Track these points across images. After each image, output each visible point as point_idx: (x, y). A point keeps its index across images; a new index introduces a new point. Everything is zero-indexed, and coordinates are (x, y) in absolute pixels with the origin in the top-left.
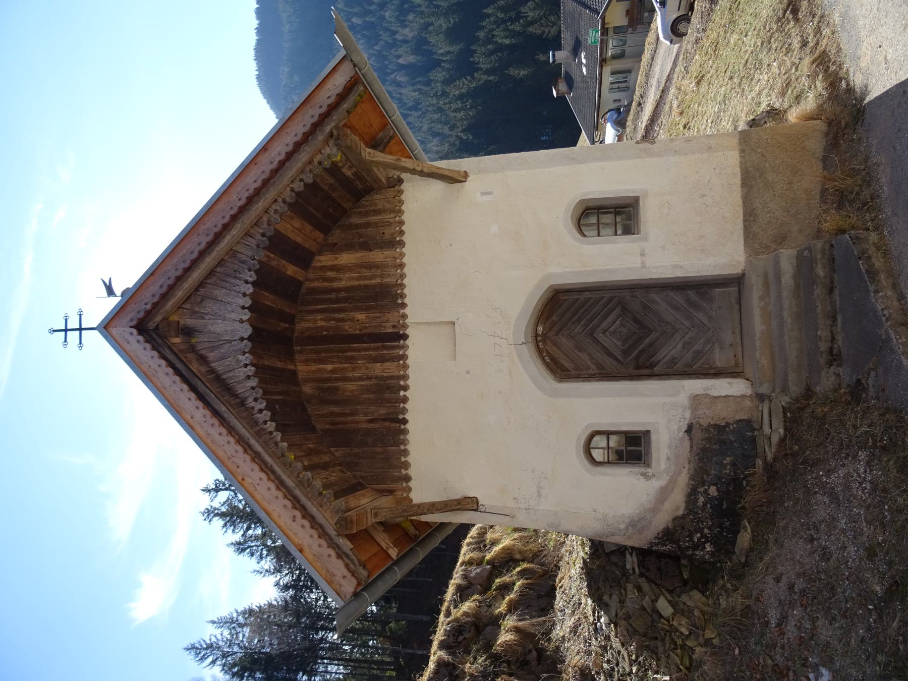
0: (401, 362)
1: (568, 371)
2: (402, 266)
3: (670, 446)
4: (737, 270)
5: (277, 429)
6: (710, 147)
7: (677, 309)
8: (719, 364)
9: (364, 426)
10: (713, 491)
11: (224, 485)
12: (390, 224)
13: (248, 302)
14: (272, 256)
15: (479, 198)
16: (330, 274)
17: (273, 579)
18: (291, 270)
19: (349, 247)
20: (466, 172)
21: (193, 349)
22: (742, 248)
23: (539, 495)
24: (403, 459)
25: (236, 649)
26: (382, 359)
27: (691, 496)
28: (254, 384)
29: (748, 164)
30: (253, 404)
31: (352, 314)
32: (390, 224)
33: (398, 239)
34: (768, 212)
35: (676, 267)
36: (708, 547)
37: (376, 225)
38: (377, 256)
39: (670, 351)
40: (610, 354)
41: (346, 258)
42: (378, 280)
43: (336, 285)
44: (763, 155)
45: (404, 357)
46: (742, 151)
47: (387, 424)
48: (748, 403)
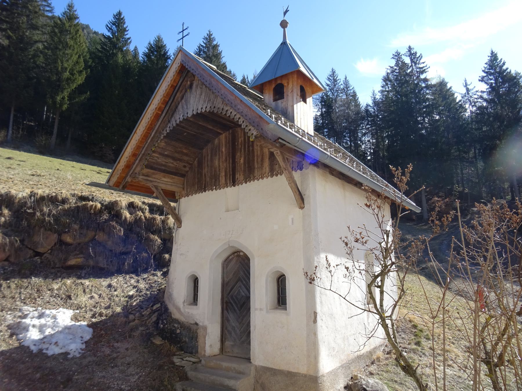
10: (178, 331)
11: (414, 58)
17: (370, 103)
23: (181, 254)
25: (336, 94)
26: (226, 175)
27: (177, 321)
31: (243, 156)
35: (255, 327)
42: (256, 167)
44: (301, 388)
46: (305, 376)
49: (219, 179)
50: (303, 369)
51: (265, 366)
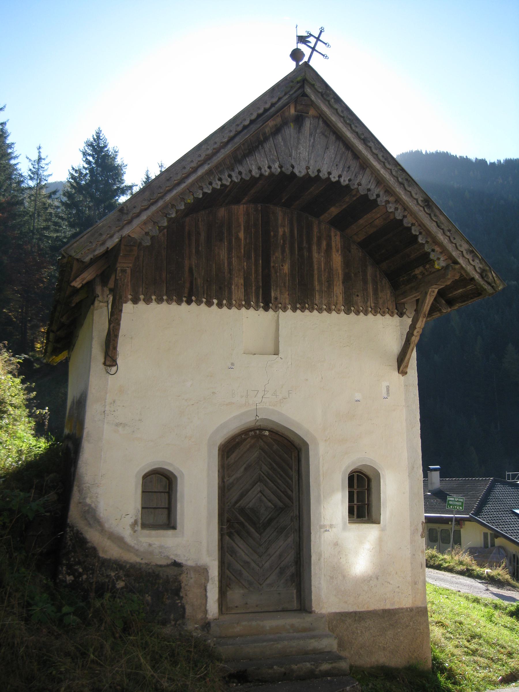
0: (244, 303)
1: (228, 457)
2: (329, 310)
3: (161, 547)
4: (315, 607)
5: (214, 189)
6: (415, 583)
7: (280, 556)
8: (229, 593)
9: (187, 262)
12: (365, 302)
13: (324, 175)
14: (355, 198)
15: (385, 384)
16: (324, 243)
18: (334, 211)
19: (347, 264)
20: (406, 373)
21: (285, 123)
22: (333, 611)
23: (117, 425)
24: (154, 297)
26: (247, 285)
27: (107, 564)
28: (254, 173)
29: (401, 614)
30: (236, 171)
32: (365, 302)
33: (352, 308)
34: (362, 632)
36: (70, 578)
37: (365, 289)
38: (338, 289)
39: (242, 549)
40: (242, 496)
41: (337, 259)
42: (317, 288)
43: (315, 248)
44: (407, 626)
45: (248, 306)
46: (411, 610)
47: (187, 285)
48: (200, 616)
49: (230, 289)
50: (406, 602)
51: (343, 610)
